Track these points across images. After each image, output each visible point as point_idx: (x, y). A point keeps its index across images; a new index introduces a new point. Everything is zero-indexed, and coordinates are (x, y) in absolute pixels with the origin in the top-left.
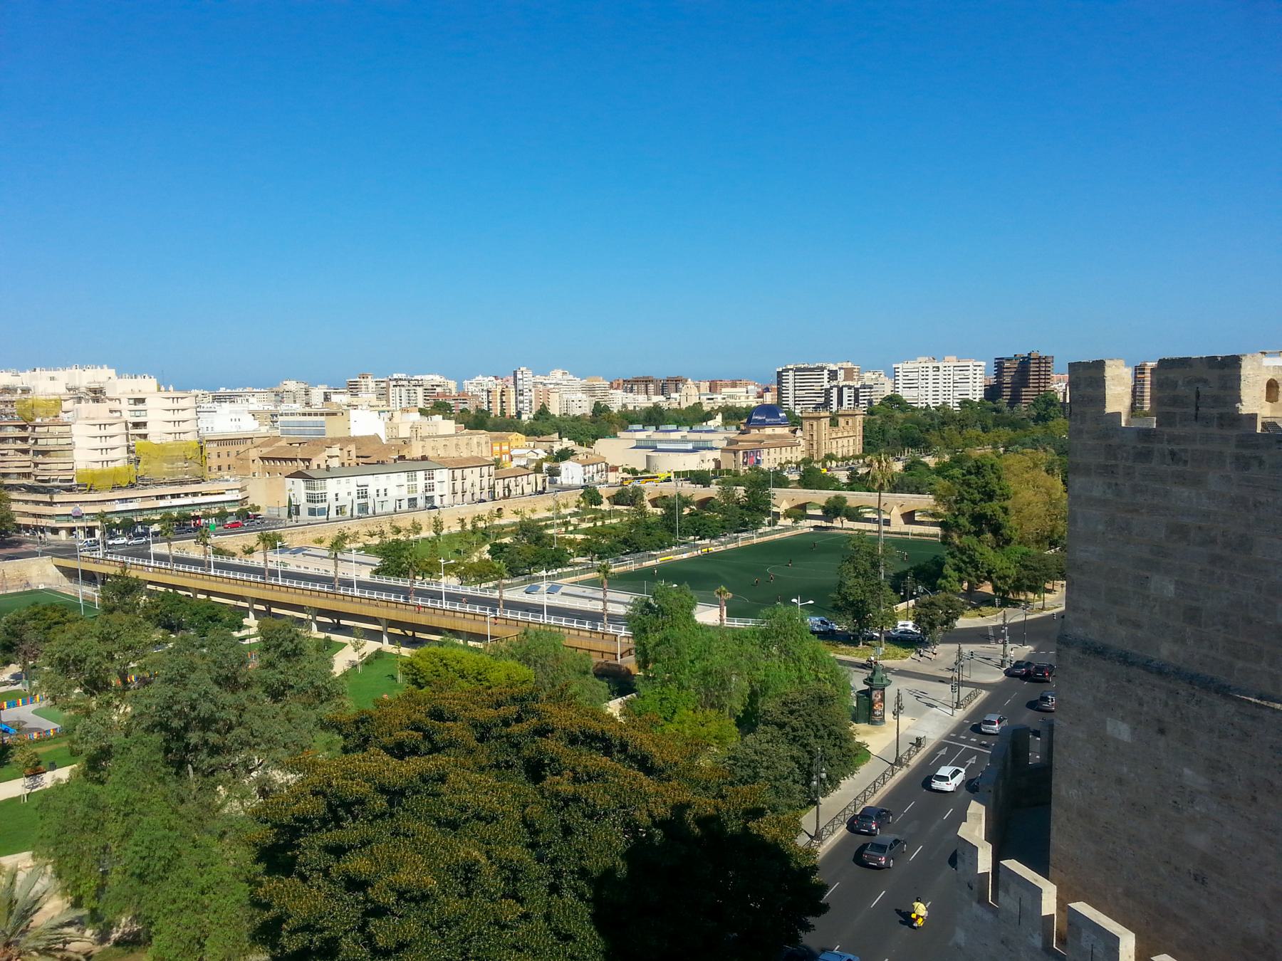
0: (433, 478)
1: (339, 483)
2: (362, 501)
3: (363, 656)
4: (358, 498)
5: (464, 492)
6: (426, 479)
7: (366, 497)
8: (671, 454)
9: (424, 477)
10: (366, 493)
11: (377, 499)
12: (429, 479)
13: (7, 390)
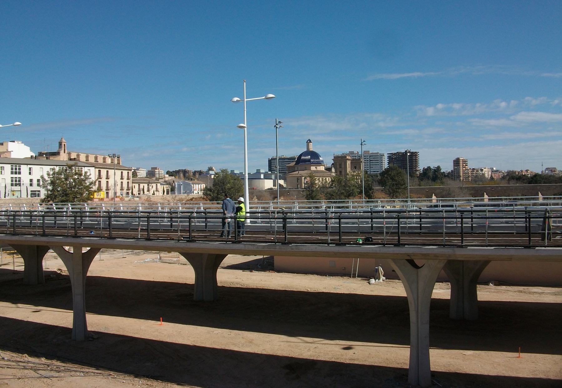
0: (20, 173)
1: (434, 350)
2: (127, 191)
3: (26, 239)
4: (12, 185)
5: (108, 189)
6: (12, 173)
7: (20, 185)
8: (244, 163)
9: (10, 170)
10: (20, 181)
11: (30, 188)
12: (16, 173)
13: (561, 198)
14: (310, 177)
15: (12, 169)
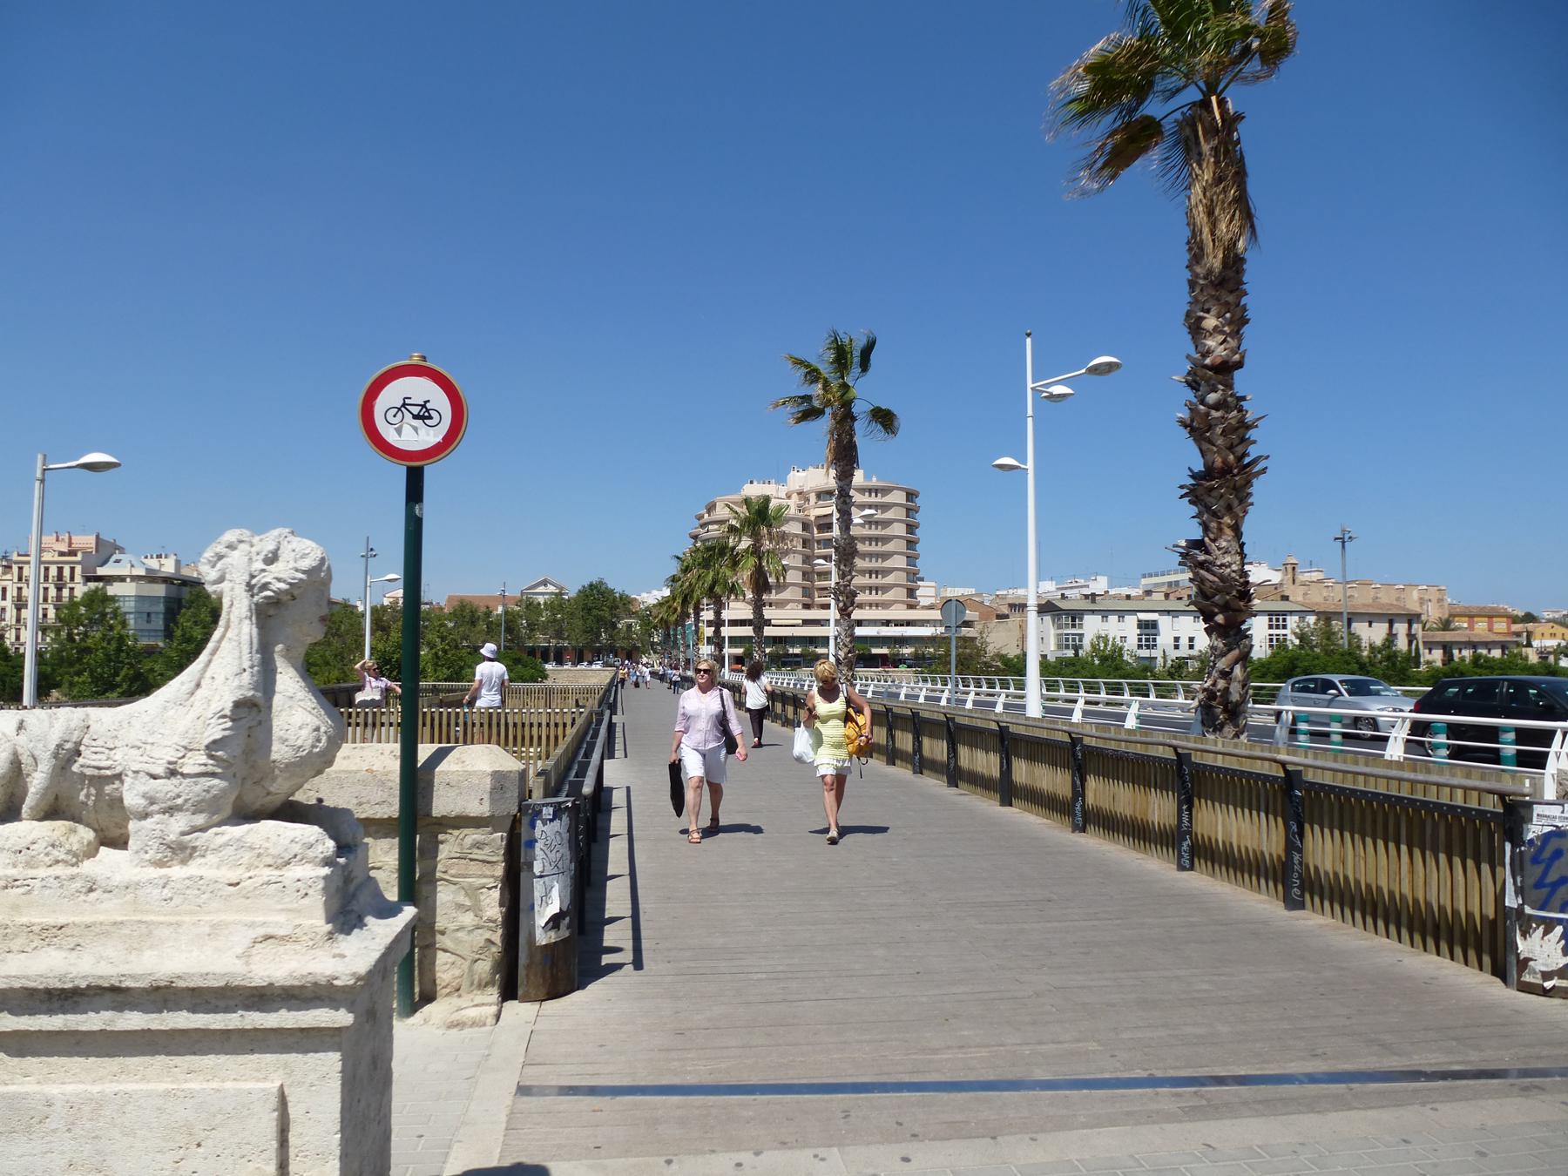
6: (1271, 627)
12: (1278, 627)
14: (1202, 662)
15: (1271, 620)
